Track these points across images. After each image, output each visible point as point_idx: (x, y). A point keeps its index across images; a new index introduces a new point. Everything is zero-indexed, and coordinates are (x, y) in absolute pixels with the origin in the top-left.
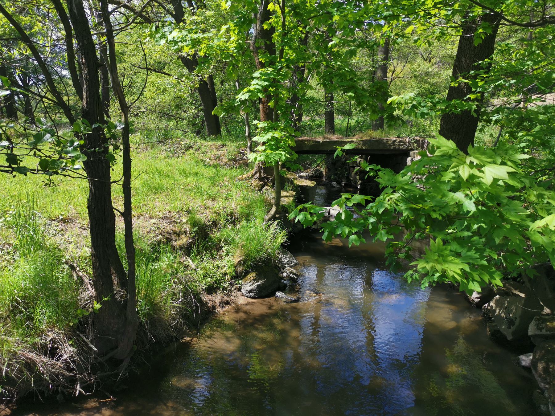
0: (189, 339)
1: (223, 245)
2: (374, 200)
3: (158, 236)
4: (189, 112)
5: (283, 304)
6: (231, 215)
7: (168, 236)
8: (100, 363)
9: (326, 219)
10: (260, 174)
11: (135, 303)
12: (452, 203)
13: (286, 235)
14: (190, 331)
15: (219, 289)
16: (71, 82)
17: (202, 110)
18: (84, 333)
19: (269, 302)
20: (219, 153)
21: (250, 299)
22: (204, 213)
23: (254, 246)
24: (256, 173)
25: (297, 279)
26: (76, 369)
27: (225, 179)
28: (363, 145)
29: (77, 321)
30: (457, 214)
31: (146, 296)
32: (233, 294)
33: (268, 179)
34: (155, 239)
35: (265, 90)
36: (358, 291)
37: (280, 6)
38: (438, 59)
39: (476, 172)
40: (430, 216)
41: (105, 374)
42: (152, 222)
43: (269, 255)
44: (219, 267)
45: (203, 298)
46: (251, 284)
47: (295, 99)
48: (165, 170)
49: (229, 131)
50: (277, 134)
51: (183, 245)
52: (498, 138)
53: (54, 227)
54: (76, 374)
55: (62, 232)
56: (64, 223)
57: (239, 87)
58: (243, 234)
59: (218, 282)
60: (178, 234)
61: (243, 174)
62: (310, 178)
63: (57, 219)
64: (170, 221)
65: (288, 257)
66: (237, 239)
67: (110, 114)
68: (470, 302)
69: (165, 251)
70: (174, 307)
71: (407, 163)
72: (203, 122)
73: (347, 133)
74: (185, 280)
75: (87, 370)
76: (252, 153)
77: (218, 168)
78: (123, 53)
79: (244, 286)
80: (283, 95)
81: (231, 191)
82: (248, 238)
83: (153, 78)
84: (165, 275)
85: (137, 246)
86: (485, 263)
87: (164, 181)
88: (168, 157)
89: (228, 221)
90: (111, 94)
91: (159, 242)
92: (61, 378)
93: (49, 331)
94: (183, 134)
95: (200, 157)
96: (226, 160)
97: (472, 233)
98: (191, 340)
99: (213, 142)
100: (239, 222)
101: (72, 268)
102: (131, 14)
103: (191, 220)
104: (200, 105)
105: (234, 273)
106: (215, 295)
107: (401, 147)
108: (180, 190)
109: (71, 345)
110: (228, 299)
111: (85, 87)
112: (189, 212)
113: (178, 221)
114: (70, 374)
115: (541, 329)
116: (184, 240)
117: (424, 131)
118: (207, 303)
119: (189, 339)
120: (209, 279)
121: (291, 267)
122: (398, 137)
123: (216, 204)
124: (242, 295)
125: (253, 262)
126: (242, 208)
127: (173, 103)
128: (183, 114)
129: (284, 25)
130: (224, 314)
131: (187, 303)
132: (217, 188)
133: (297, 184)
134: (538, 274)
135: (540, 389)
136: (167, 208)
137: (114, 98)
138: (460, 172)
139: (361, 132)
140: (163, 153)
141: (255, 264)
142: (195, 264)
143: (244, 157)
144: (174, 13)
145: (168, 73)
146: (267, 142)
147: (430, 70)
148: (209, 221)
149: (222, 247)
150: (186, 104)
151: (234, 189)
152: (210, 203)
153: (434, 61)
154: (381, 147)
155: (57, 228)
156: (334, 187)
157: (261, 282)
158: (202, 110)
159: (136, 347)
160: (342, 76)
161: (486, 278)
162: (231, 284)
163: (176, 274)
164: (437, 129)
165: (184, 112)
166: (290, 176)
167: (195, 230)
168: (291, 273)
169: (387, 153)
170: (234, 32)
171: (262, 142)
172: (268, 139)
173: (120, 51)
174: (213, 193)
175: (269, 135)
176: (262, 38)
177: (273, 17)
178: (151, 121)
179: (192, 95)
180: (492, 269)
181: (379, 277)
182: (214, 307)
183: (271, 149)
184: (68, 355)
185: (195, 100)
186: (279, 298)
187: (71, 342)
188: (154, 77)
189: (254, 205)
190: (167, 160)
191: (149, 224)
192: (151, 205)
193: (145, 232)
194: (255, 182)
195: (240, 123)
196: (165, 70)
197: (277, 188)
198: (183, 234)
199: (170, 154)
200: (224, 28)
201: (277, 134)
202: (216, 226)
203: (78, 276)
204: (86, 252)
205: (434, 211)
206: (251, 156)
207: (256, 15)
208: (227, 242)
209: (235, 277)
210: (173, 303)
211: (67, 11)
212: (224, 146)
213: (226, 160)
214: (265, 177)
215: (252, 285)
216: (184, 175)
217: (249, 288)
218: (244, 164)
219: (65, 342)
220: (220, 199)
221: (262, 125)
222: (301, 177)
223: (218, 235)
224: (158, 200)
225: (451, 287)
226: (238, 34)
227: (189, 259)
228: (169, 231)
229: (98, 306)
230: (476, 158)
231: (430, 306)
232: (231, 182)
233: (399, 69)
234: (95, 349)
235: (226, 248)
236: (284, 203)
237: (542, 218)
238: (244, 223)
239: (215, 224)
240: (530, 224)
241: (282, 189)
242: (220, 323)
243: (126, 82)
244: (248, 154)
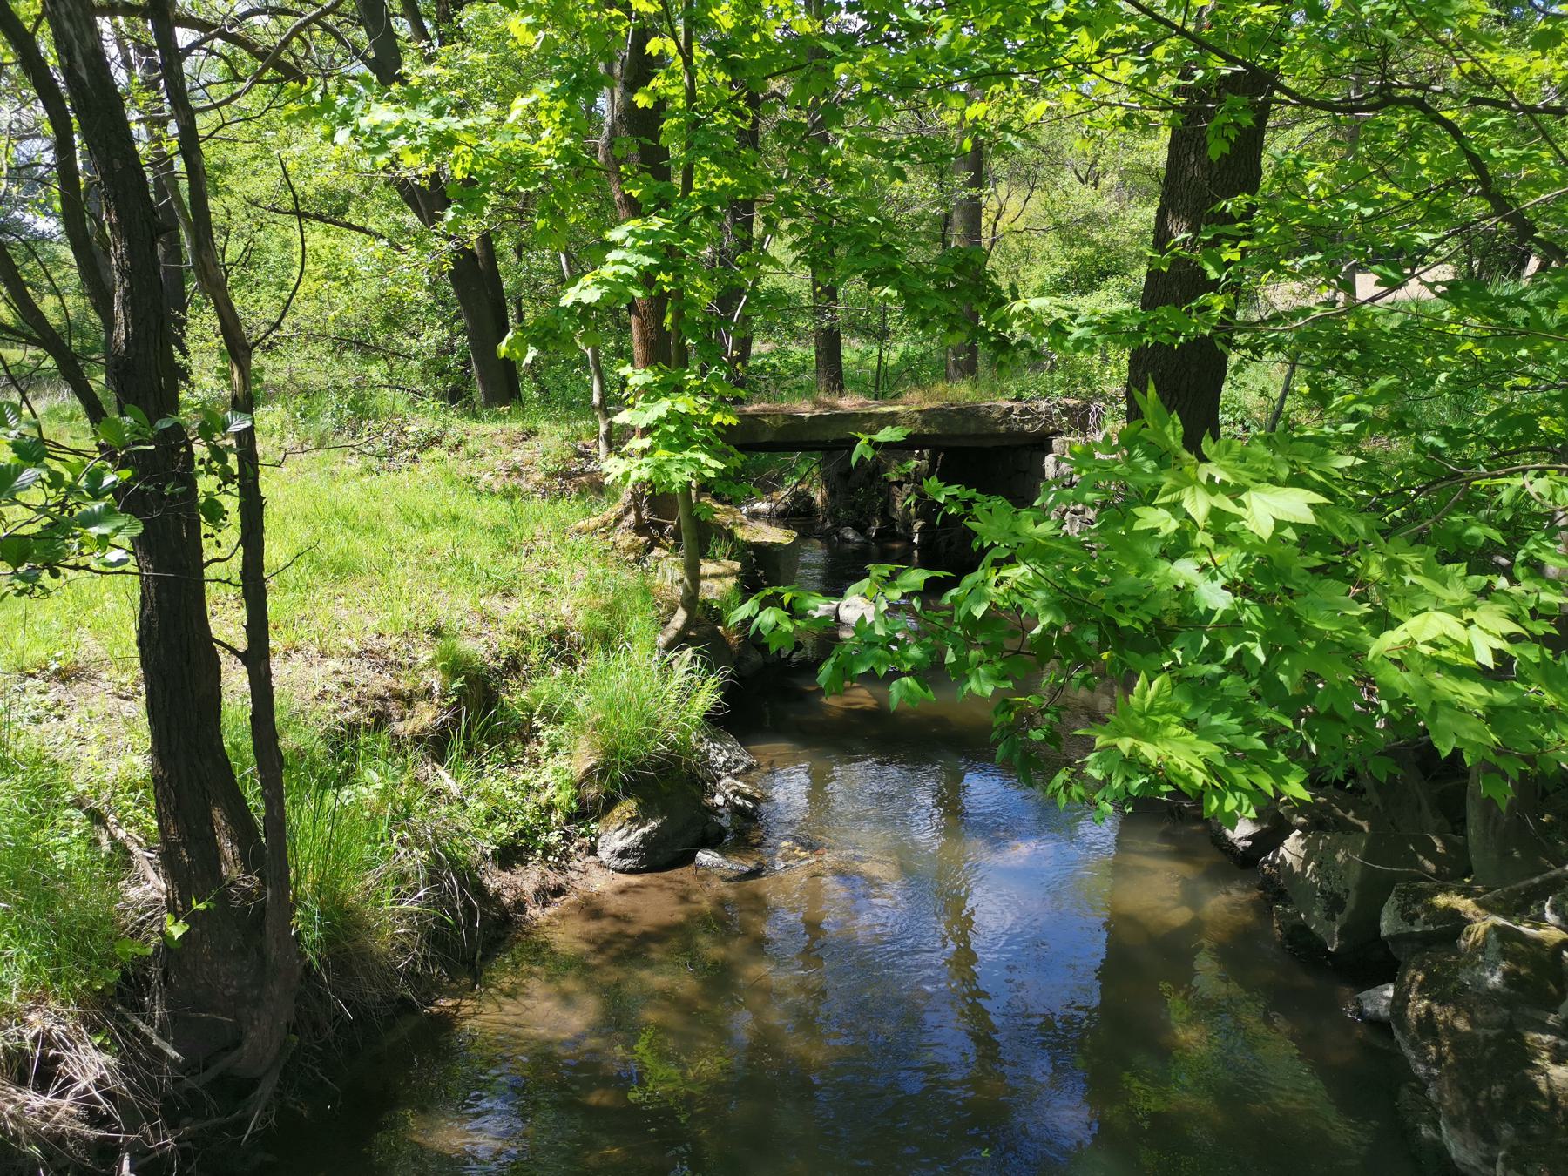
0: (450, 1003)
1: (539, 724)
2: (955, 583)
3: (347, 709)
4: (424, 337)
5: (718, 886)
6: (560, 636)
7: (379, 707)
8: (190, 1093)
9: (828, 636)
10: (638, 516)
11: (287, 908)
12: (1165, 588)
13: (721, 688)
14: (452, 980)
15: (532, 851)
16: (66, 253)
17: (463, 331)
18: (138, 1008)
19: (681, 882)
20: (517, 456)
21: (622, 876)
22: (480, 635)
23: (630, 724)
24: (627, 511)
25: (754, 809)
26: (118, 1118)
27: (538, 530)
28: (924, 422)
29: (117, 973)
30: (1182, 618)
31: (319, 889)
32: (574, 863)
33: (661, 527)
34: (339, 718)
35: (647, 278)
36: (926, 833)
37: (678, 44)
38: (1116, 179)
39: (1228, 506)
40: (1112, 623)
41: (208, 1123)
42: (330, 669)
43: (673, 745)
44: (529, 787)
45: (487, 880)
46: (623, 831)
47: (727, 299)
48: (361, 510)
49: (543, 389)
50: (684, 404)
51: (424, 730)
52: (1282, 399)
53: (33, 697)
54: (119, 1131)
55: (59, 711)
56: (63, 682)
57: (570, 269)
58: (596, 693)
59: (528, 833)
60: (408, 700)
61: (590, 515)
62: (782, 518)
63: (42, 670)
64: (381, 662)
65: (729, 750)
66: (580, 706)
67: (191, 347)
68: (1228, 847)
69: (373, 754)
70: (404, 915)
71: (1043, 470)
72: (467, 363)
73: (877, 388)
74: (434, 833)
75: (150, 1117)
76: (614, 459)
77: (517, 500)
78: (224, 168)
79: (603, 838)
80: (696, 290)
81: (557, 566)
82: (610, 704)
83: (318, 237)
84: (373, 822)
85: (287, 742)
86: (1261, 745)
87: (360, 544)
88: (369, 470)
89: (553, 653)
90: (190, 286)
91: (352, 727)
92: (71, 1146)
93: (30, 1010)
94: (411, 403)
95: (464, 468)
96: (539, 477)
97: (1223, 666)
98: (457, 1007)
99: (499, 425)
100: (584, 654)
101: (97, 818)
102: (243, 53)
103: (443, 656)
104: (457, 317)
105: (574, 805)
106: (520, 869)
107: (1027, 427)
108: (407, 569)
109: (102, 1048)
110: (561, 880)
111: (119, 292)
112: (436, 632)
113: (407, 661)
114: (100, 1133)
115: (1411, 919)
116: (425, 716)
117: (1087, 381)
118: (498, 894)
119: (450, 1003)
120: (504, 825)
121: (736, 776)
122: (1019, 398)
123: (514, 606)
124: (601, 865)
125: (628, 770)
126: (590, 615)
127: (378, 314)
128: (407, 342)
129: (691, 95)
130: (549, 924)
131: (441, 900)
132: (515, 560)
133: (745, 538)
134: (1399, 773)
135: (1417, 1079)
136: (373, 624)
137: (198, 297)
138: (1185, 505)
139: (918, 385)
140: (353, 460)
141: (634, 775)
142: (461, 784)
143: (591, 466)
144: (372, 55)
145: (360, 223)
146: (656, 428)
147: (1098, 207)
148: (498, 658)
149: (537, 730)
150: (416, 312)
151: (564, 560)
152: (495, 604)
153: (1105, 182)
154: (972, 427)
155: (43, 697)
156: (848, 541)
157: (654, 824)
158: (463, 331)
159: (295, 1039)
160: (860, 242)
161: (1266, 784)
162: (567, 837)
163: (407, 817)
164: (1119, 373)
165: (412, 335)
166: (723, 514)
167: (457, 685)
168: (736, 793)
169: (990, 444)
170: (548, 116)
171: (642, 425)
172: (660, 419)
173: (213, 159)
174: (506, 575)
175: (661, 408)
176: (631, 133)
177: (661, 72)
178: (313, 365)
179: (432, 288)
180: (1276, 757)
181: (983, 789)
182: (520, 906)
183: (670, 447)
184: (92, 1078)
185: (441, 303)
186: (705, 867)
187: (98, 1040)
188: (318, 235)
189: (624, 604)
190: (365, 480)
191: (320, 675)
192: (320, 622)
193: (309, 698)
194: (625, 538)
195: (575, 366)
196: (352, 216)
197: (688, 552)
198: (422, 699)
199: (374, 462)
200: (520, 104)
201: (684, 404)
202: (518, 670)
203: (112, 837)
204: (134, 767)
205: (1121, 609)
206: (612, 467)
207: (609, 68)
208: (550, 717)
209: (577, 814)
210: (400, 903)
211: (60, 78)
212: (530, 434)
213: (539, 477)
214: (652, 523)
215: (628, 835)
216: (419, 523)
217: (619, 845)
218: (591, 485)
219: (80, 1039)
220: (525, 592)
221: (638, 376)
222: (755, 516)
223: (524, 696)
224: (342, 601)
225: (1172, 814)
226: (563, 122)
227: (441, 771)
228: (382, 692)
229: (177, 930)
230: (1223, 468)
231: (1118, 870)
232: (555, 539)
233: (1014, 205)
234: (175, 1054)
235: (548, 732)
236: (709, 596)
237: (1401, 622)
238: (597, 659)
239: (514, 665)
240: (1366, 636)
241: (704, 555)
242: (537, 951)
243: (234, 249)
244: (602, 457)
